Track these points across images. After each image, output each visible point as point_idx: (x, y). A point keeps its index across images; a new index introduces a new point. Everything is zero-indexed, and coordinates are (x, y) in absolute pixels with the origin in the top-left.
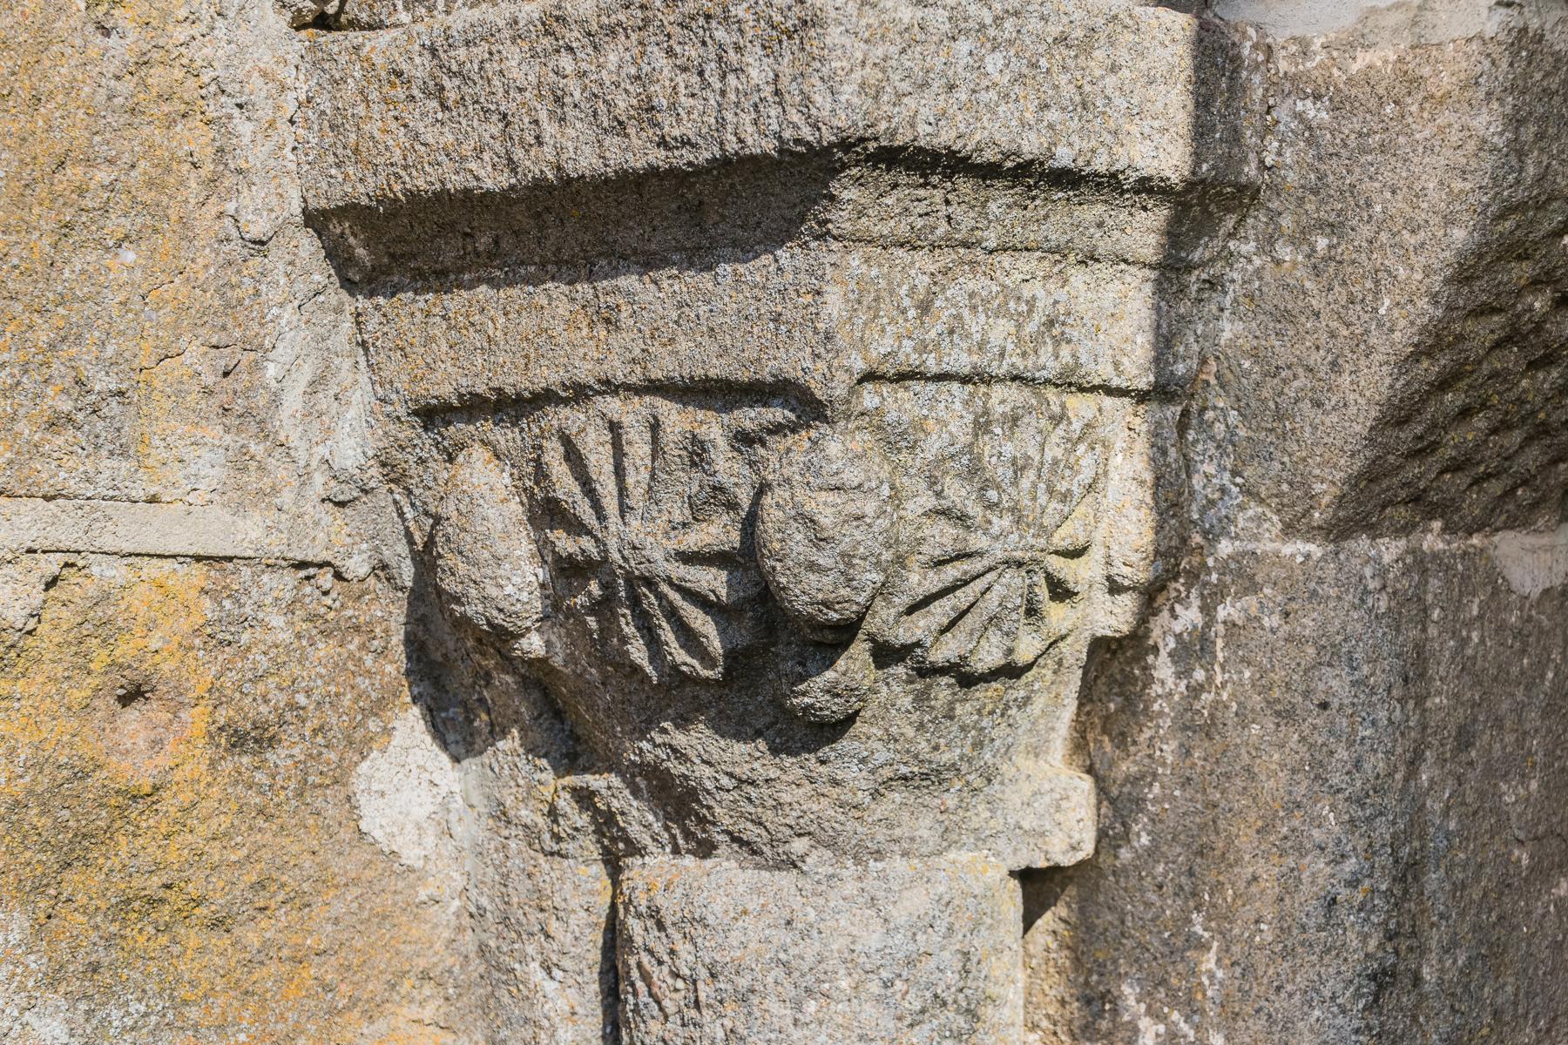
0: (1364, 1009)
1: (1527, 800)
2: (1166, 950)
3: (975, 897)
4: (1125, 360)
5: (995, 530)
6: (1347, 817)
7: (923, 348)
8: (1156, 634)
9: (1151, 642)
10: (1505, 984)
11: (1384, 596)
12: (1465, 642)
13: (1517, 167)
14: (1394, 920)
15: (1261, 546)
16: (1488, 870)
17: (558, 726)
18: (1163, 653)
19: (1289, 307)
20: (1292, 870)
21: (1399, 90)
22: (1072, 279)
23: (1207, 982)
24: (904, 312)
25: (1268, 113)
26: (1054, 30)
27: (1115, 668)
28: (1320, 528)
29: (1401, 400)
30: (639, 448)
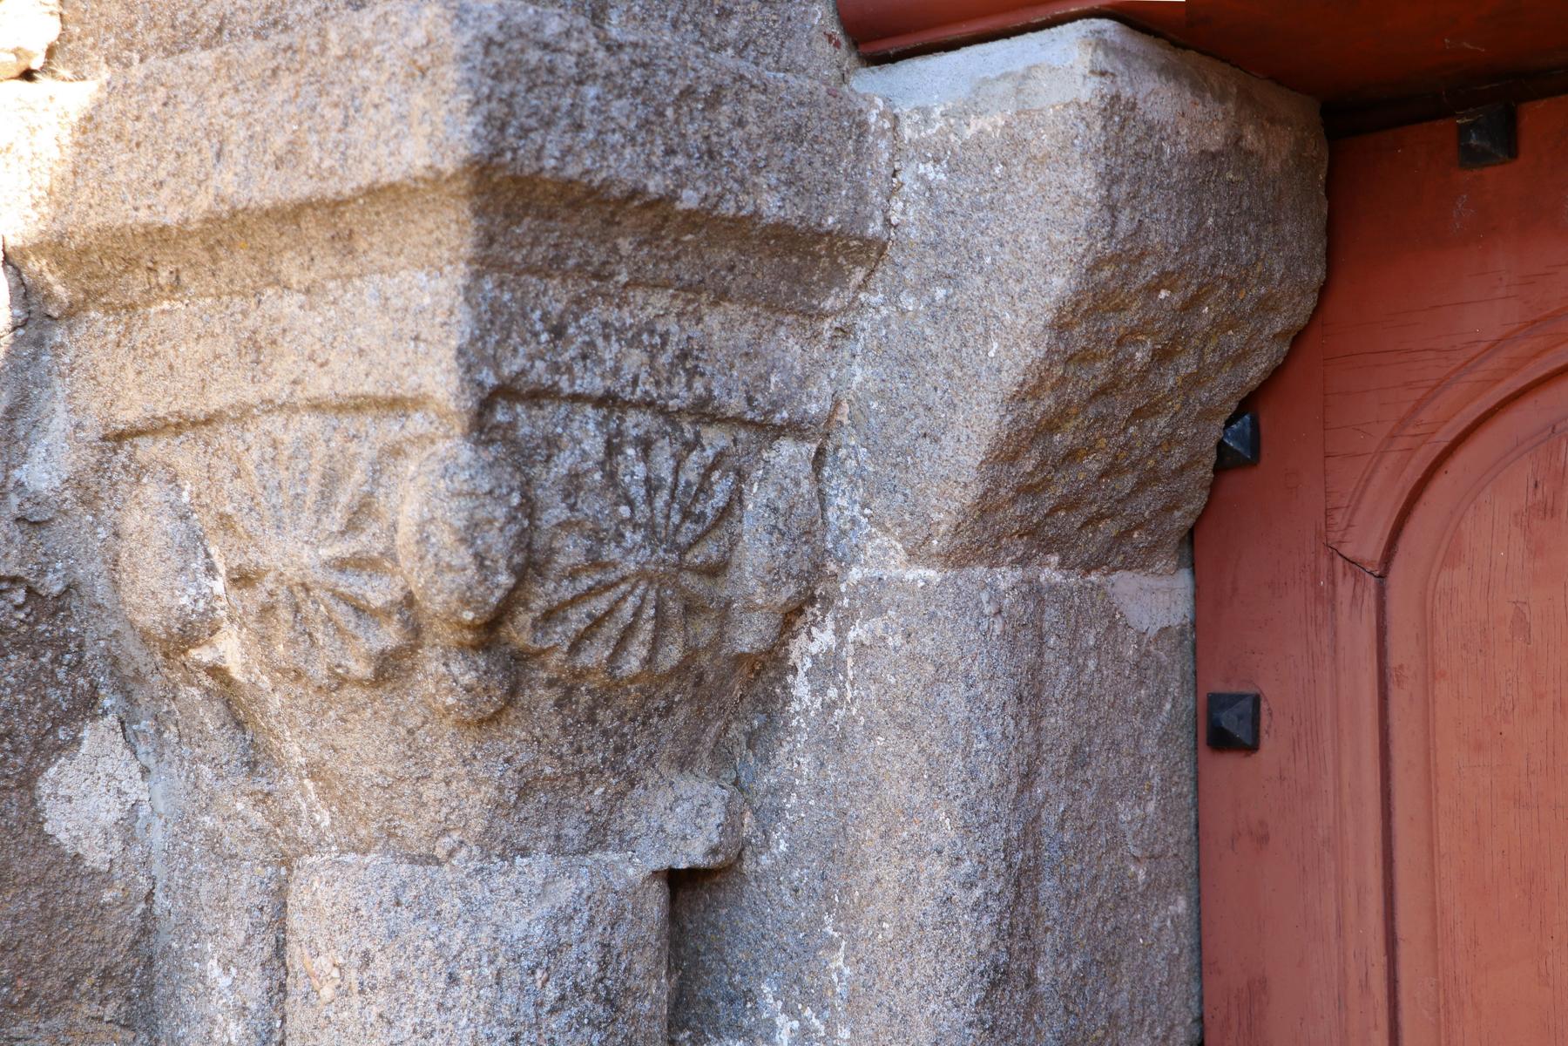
0: (977, 1004)
1: (1144, 819)
2: (800, 950)
3: (616, 893)
4: (759, 396)
5: (628, 544)
6: (962, 823)
7: (555, 368)
8: (794, 655)
9: (790, 663)
10: (1120, 991)
11: (999, 620)
12: (1081, 669)
13: (1109, 221)
14: (1007, 922)
15: (887, 572)
16: (1103, 882)
17: (239, 736)
18: (801, 673)
19: (911, 352)
20: (912, 872)
21: (1008, 152)
22: (706, 318)
23: (836, 980)
24: (536, 335)
25: (894, 175)
26: (681, 83)
27: (759, 687)
28: (939, 555)
29: (1008, 436)
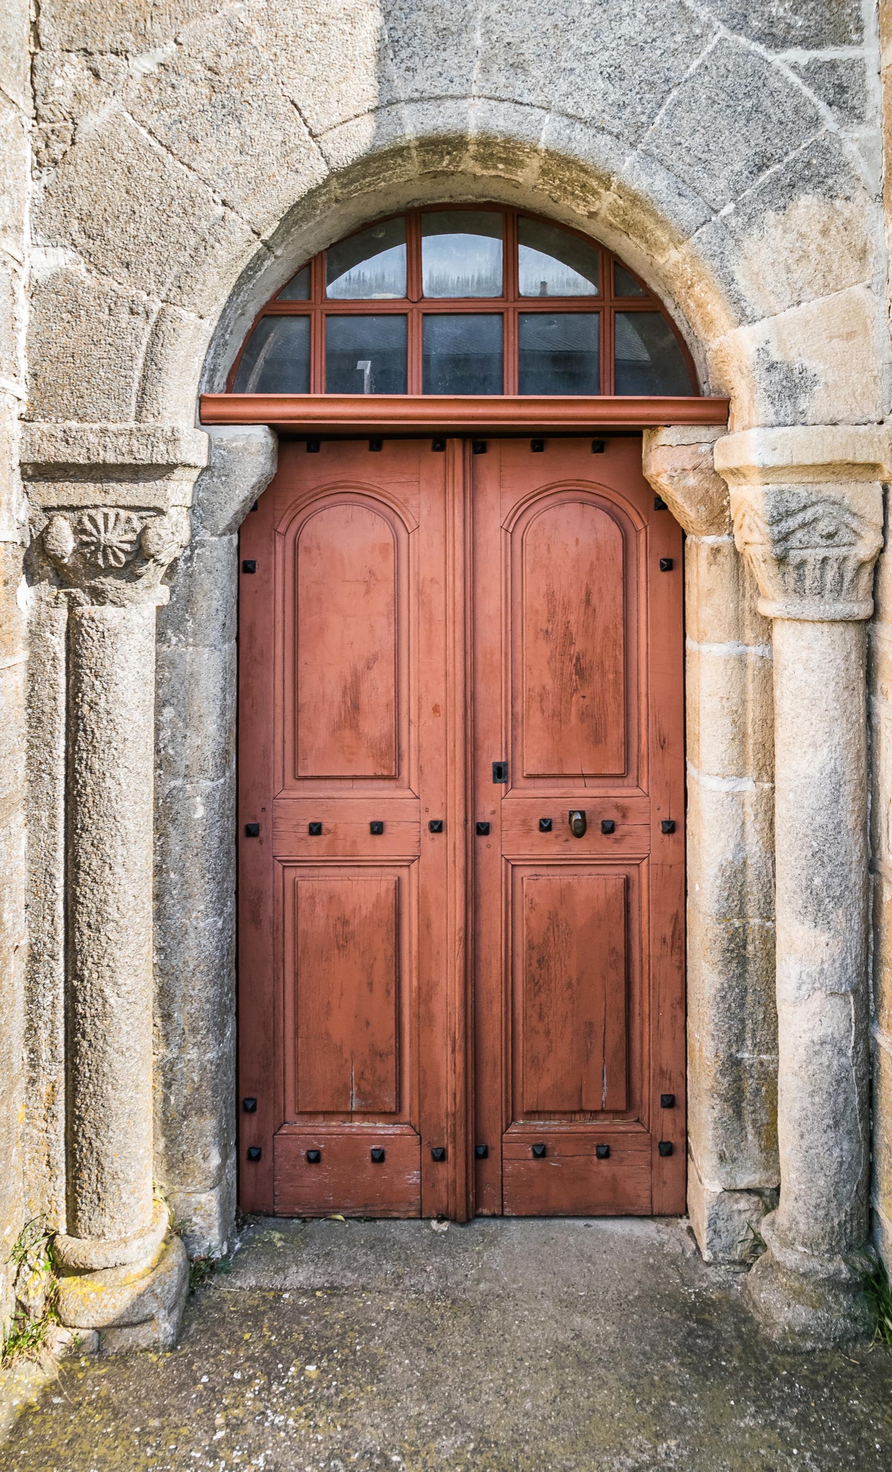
30: (112, 519)
